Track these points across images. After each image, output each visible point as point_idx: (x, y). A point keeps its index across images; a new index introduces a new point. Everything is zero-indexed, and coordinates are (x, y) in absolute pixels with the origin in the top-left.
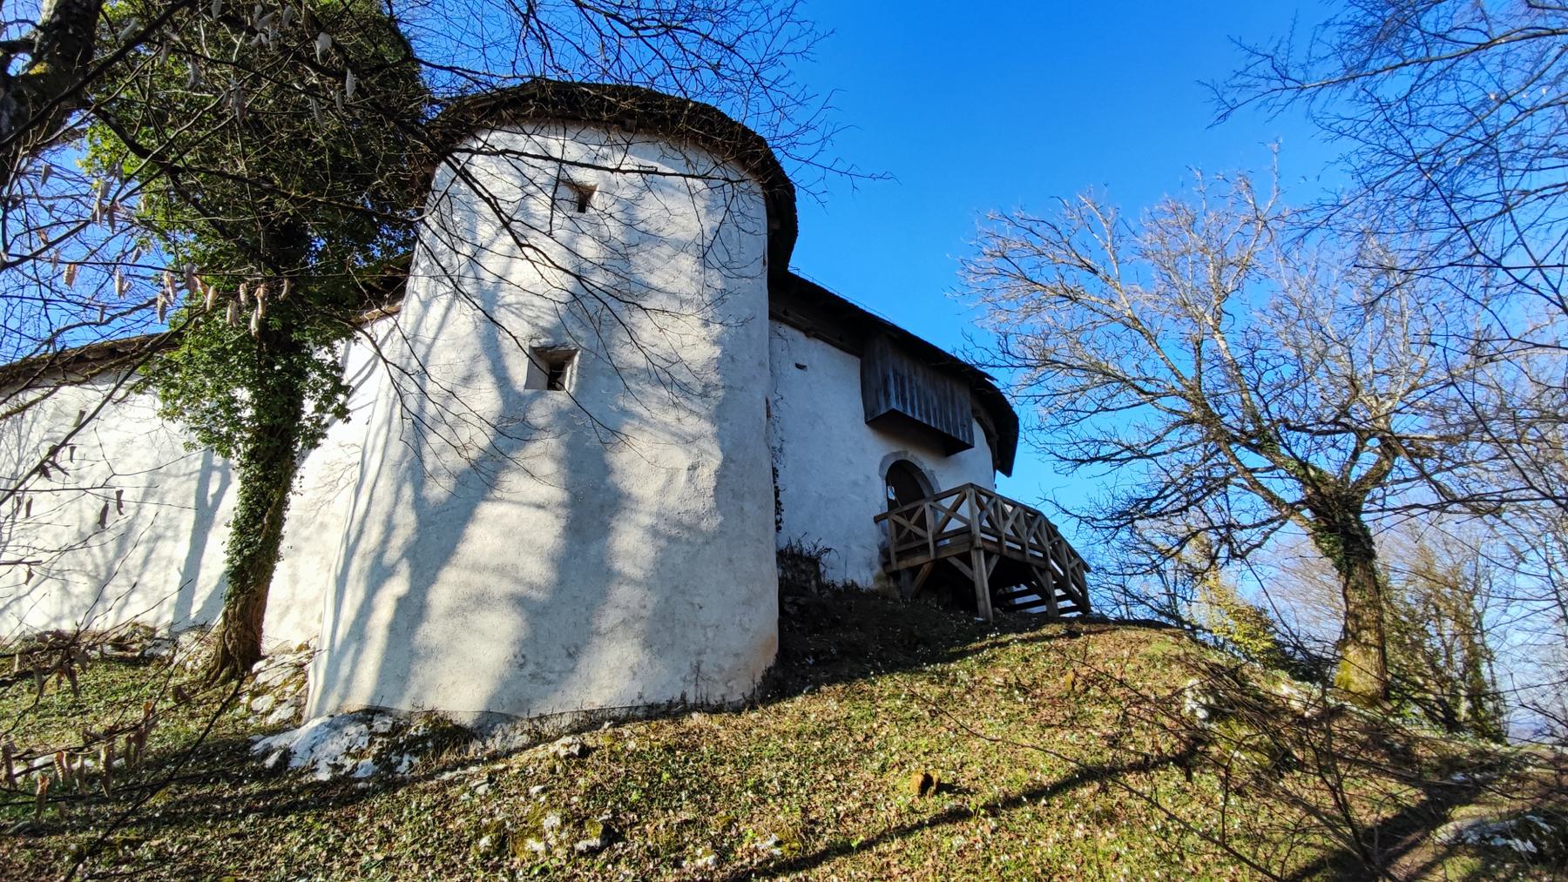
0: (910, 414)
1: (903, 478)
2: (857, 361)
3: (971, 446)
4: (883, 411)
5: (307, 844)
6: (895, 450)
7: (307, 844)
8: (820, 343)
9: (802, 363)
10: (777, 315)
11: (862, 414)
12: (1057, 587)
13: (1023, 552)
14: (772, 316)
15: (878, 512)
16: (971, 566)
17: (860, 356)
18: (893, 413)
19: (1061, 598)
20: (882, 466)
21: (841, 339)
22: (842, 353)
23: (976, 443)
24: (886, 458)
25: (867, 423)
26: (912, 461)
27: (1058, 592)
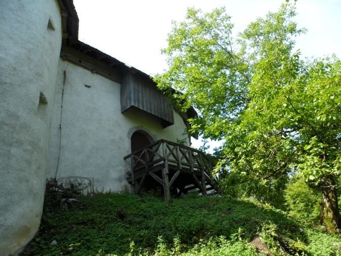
0: (141, 108)
1: (139, 140)
2: (120, 85)
3: (172, 124)
4: (129, 107)
5: (234, 252)
6: (136, 125)
7: (234, 252)
8: (99, 76)
9: (88, 85)
10: (64, 56)
11: (120, 107)
12: (207, 184)
13: (190, 170)
14: (61, 56)
15: (126, 154)
16: (161, 178)
17: (120, 83)
18: (132, 107)
19: (209, 189)
20: (129, 133)
21: (110, 75)
22: (111, 81)
23: (175, 121)
24: (131, 129)
25: (122, 113)
26: (146, 130)
27: (208, 186)
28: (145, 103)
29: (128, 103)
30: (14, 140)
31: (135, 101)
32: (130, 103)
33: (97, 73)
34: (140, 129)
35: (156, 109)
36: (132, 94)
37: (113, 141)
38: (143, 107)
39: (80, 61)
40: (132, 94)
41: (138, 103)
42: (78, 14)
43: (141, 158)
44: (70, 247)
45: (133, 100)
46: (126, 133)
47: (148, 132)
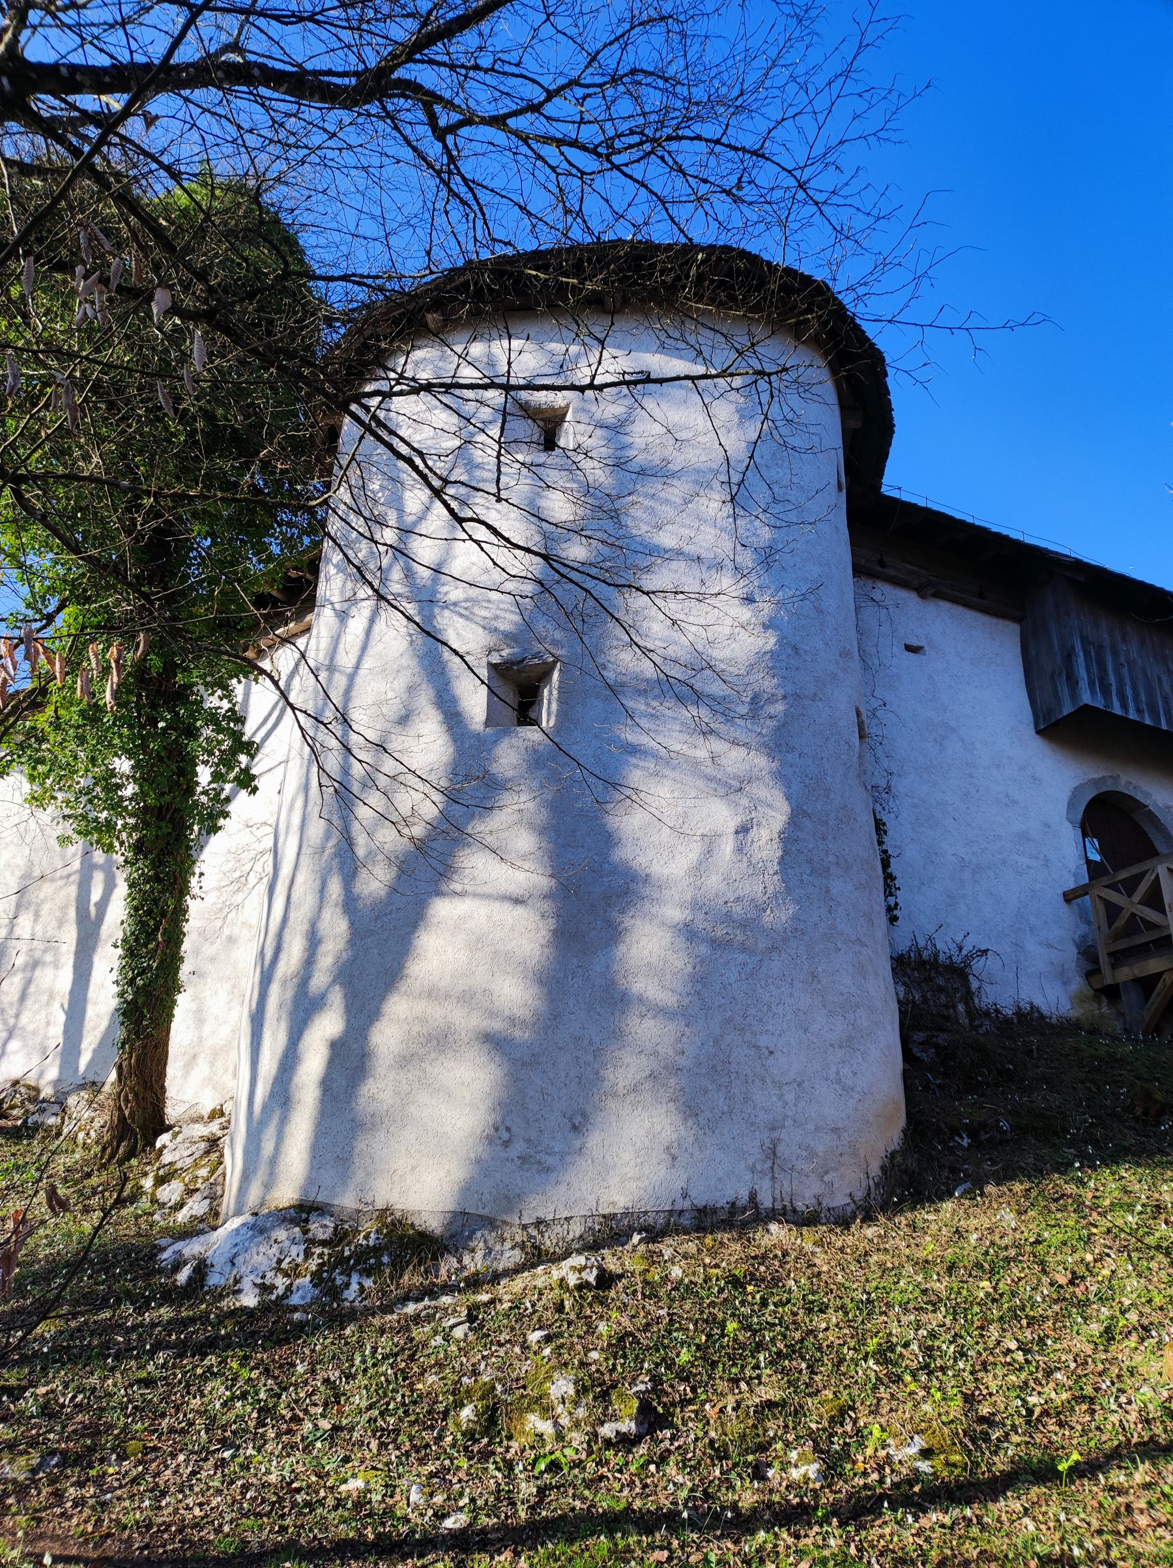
2: (1014, 629)
4: (1067, 709)
6: (1096, 775)
8: (945, 605)
9: (915, 642)
14: (858, 570)
20: (1071, 805)
21: (981, 596)
24: (1077, 791)
25: (1038, 733)
28: (1129, 692)
29: (1065, 693)
30: (831, 859)
31: (1091, 684)
32: (1074, 695)
33: (939, 595)
34: (1108, 787)
35: (1143, 698)
36: (1081, 659)
37: (1023, 837)
38: (1124, 706)
39: (882, 563)
40: (1081, 659)
41: (1106, 693)
42: (892, 397)
43: (1145, 902)
44: (412, 1255)
45: (1084, 684)
46: (1063, 807)
47: (1139, 797)
